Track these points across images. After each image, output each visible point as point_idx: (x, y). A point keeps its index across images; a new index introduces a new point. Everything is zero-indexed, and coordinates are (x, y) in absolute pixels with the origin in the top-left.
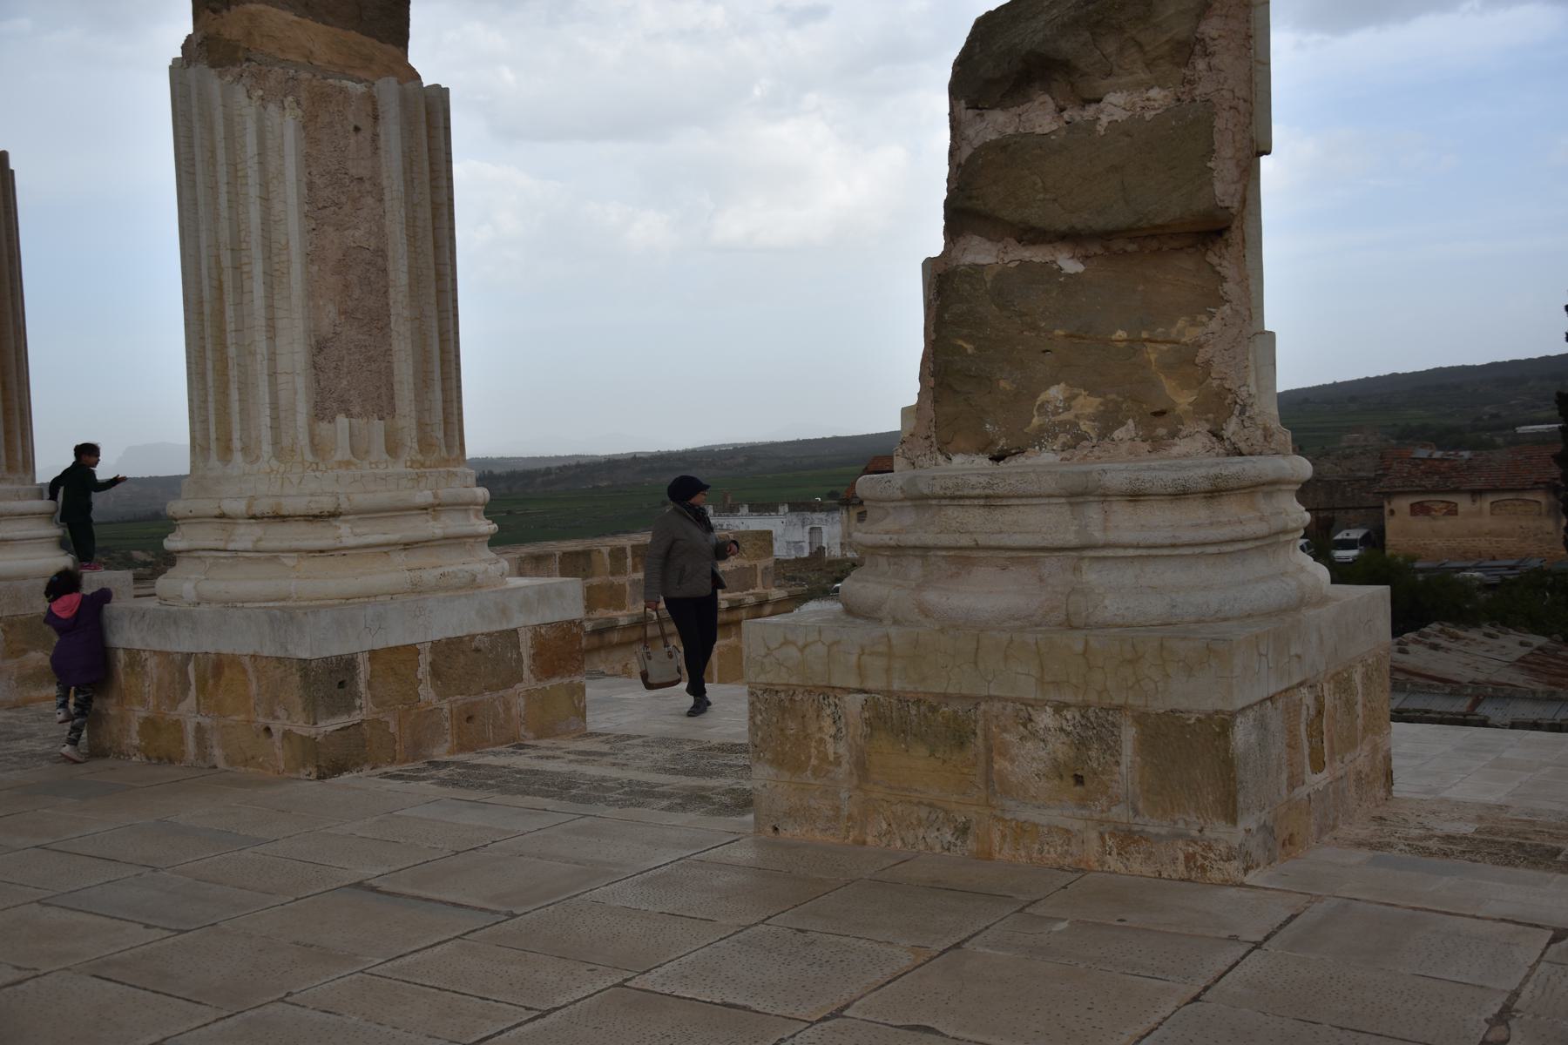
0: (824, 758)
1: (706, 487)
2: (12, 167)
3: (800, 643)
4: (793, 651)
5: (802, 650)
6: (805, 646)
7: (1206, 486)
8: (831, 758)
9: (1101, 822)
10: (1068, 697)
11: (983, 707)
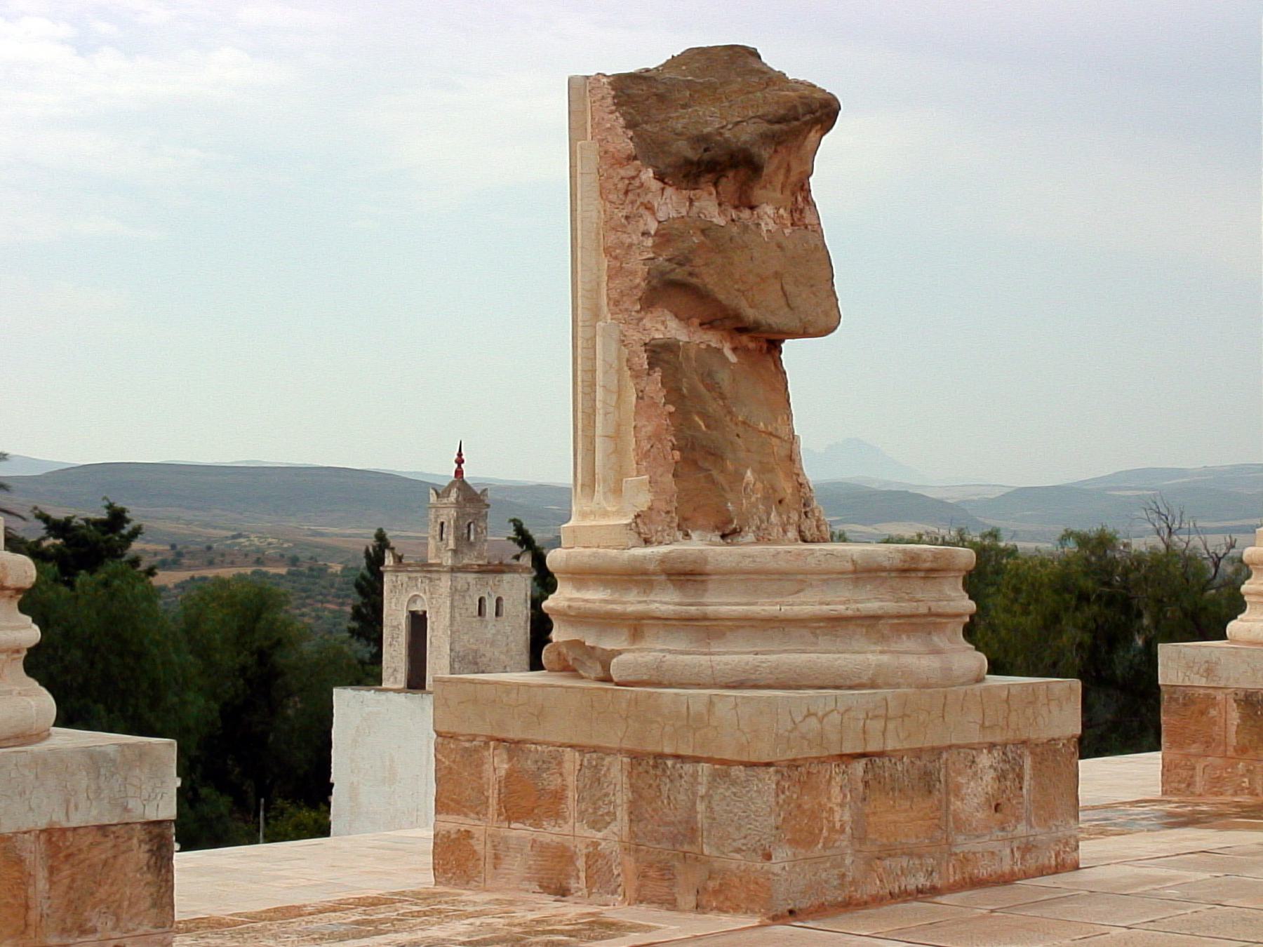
0: (832, 829)
1: (380, 531)
2: (332, 779)
3: (820, 714)
4: (813, 722)
5: (821, 721)
6: (826, 715)
7: (897, 563)
8: (838, 825)
9: (1013, 839)
10: (998, 738)
11: (945, 755)
